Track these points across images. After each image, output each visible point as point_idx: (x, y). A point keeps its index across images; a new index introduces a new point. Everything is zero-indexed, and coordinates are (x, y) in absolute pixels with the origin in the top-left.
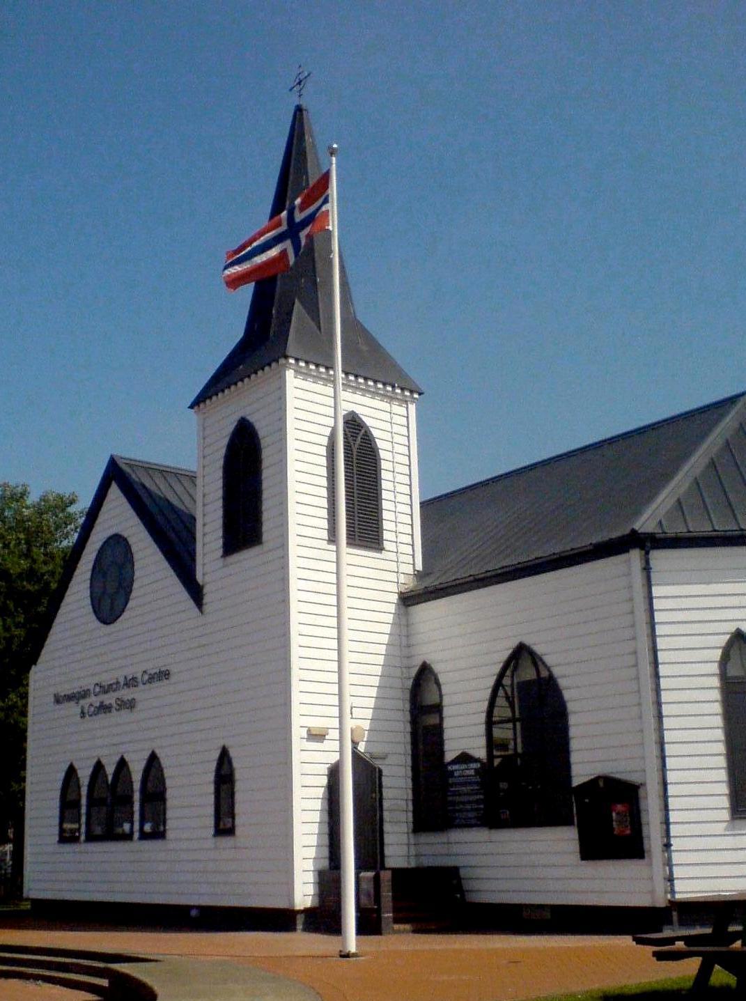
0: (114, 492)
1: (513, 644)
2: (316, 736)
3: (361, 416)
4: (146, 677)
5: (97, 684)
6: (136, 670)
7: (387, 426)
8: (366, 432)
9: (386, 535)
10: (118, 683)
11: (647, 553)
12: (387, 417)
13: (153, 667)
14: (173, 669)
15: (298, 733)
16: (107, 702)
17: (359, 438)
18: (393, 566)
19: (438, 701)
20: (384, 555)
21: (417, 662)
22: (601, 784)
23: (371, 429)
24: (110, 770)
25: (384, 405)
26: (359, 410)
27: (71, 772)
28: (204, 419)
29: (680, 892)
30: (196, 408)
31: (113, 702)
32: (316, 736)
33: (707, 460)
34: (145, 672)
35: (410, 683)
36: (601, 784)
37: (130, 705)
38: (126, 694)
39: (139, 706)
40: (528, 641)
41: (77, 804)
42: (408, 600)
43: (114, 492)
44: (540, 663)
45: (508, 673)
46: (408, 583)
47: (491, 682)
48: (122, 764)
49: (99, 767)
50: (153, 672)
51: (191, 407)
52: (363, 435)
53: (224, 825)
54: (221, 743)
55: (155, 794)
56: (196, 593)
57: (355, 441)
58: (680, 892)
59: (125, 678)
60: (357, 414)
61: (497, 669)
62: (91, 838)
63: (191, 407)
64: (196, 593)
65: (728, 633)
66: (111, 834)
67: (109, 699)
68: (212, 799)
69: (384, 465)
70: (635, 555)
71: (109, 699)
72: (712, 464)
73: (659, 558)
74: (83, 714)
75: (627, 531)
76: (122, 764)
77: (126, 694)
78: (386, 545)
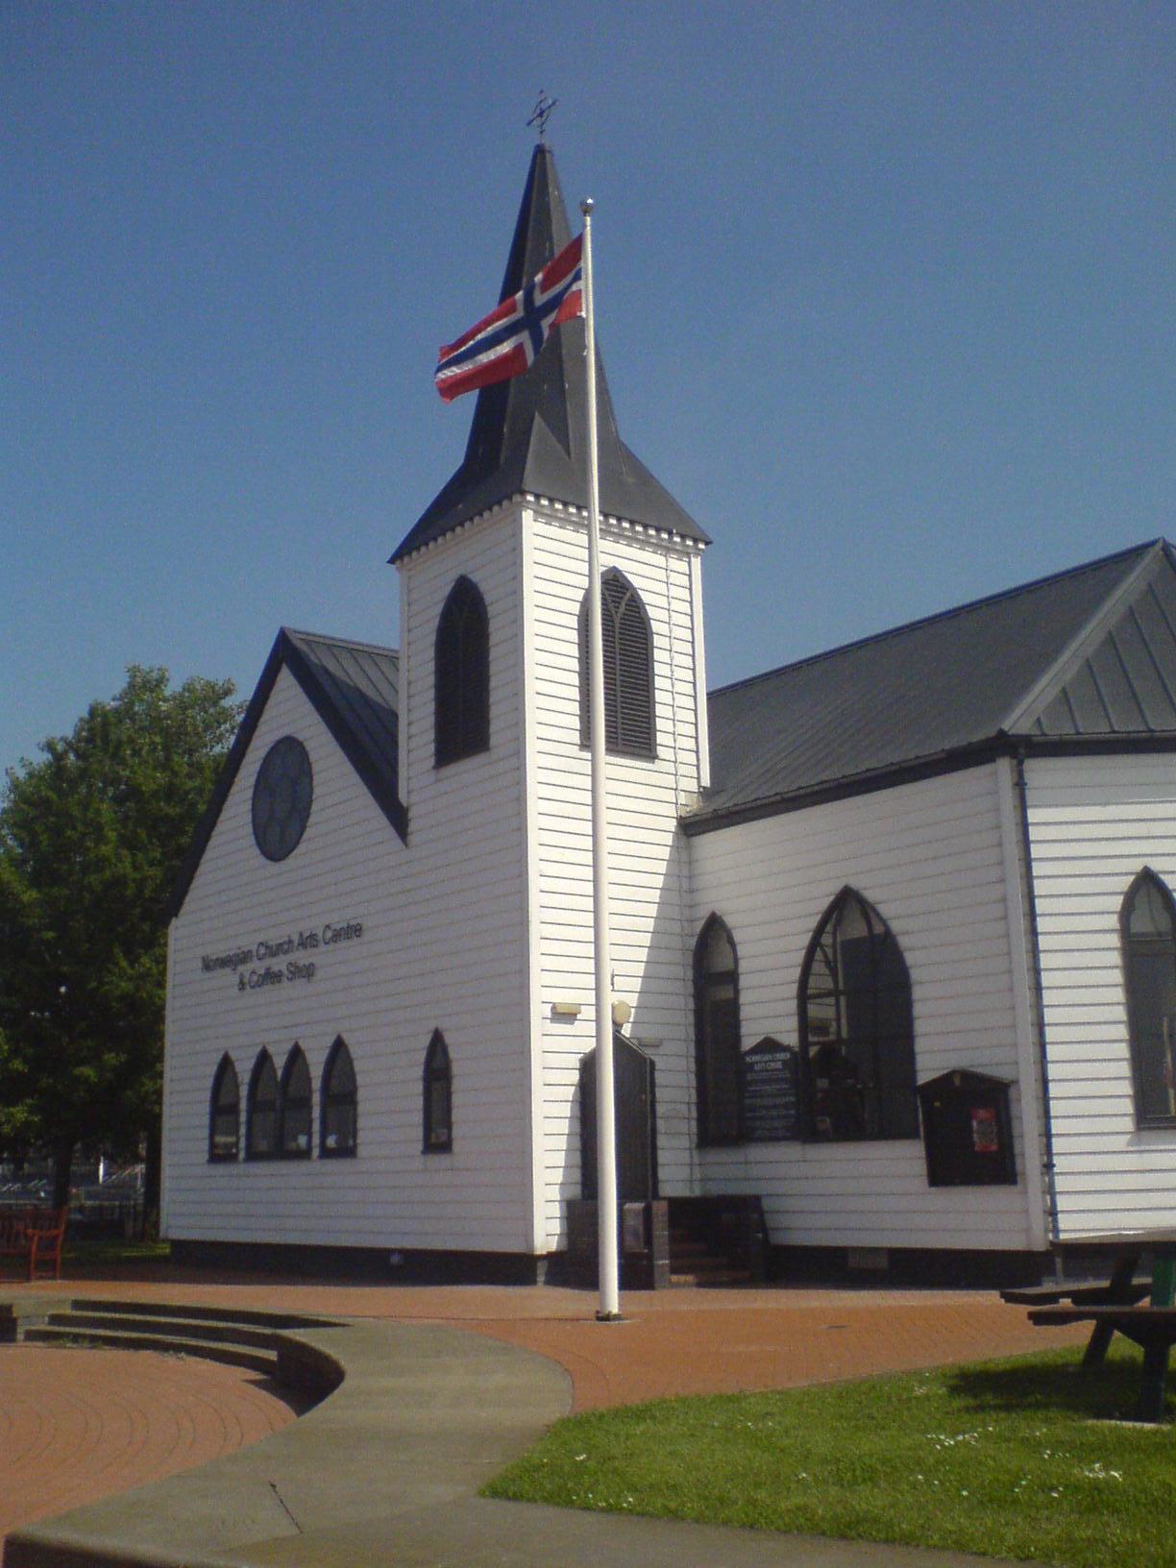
0: (286, 679)
1: (835, 887)
2: (564, 1015)
3: (626, 574)
4: (329, 934)
5: (262, 944)
6: (316, 925)
7: (662, 588)
8: (632, 596)
9: (660, 738)
10: (290, 942)
11: (1021, 763)
12: (661, 574)
13: (338, 920)
14: (367, 923)
15: (539, 1011)
16: (275, 969)
17: (623, 604)
18: (670, 781)
19: (730, 966)
20: (658, 765)
21: (704, 913)
22: (957, 1081)
23: (640, 592)
24: (280, 1062)
25: (659, 559)
26: (623, 565)
27: (226, 1064)
28: (409, 578)
29: (1065, 1231)
30: (398, 563)
31: (283, 967)
32: (564, 1015)
33: (1102, 635)
34: (328, 927)
35: (693, 942)
36: (957, 1081)
37: (307, 972)
38: (302, 957)
39: (320, 974)
40: (857, 883)
41: (233, 1109)
42: (690, 828)
43: (286, 679)
44: (872, 914)
45: (829, 928)
46: (690, 803)
47: (805, 940)
48: (296, 1054)
49: (264, 1058)
50: (338, 927)
51: (392, 561)
52: (629, 600)
53: (437, 1137)
54: (432, 1025)
55: (342, 1094)
56: (398, 817)
57: (618, 608)
58: (1065, 1231)
59: (301, 934)
60: (620, 571)
61: (813, 922)
62: (253, 1156)
63: (392, 561)
64: (398, 817)
65: (1131, 874)
66: (281, 1150)
67: (279, 964)
68: (419, 1102)
69: (657, 641)
70: (1004, 766)
71: (279, 964)
72: (1110, 640)
73: (1041, 772)
74: (242, 986)
75: (992, 732)
76: (296, 1054)
77: (302, 957)
78: (661, 751)
